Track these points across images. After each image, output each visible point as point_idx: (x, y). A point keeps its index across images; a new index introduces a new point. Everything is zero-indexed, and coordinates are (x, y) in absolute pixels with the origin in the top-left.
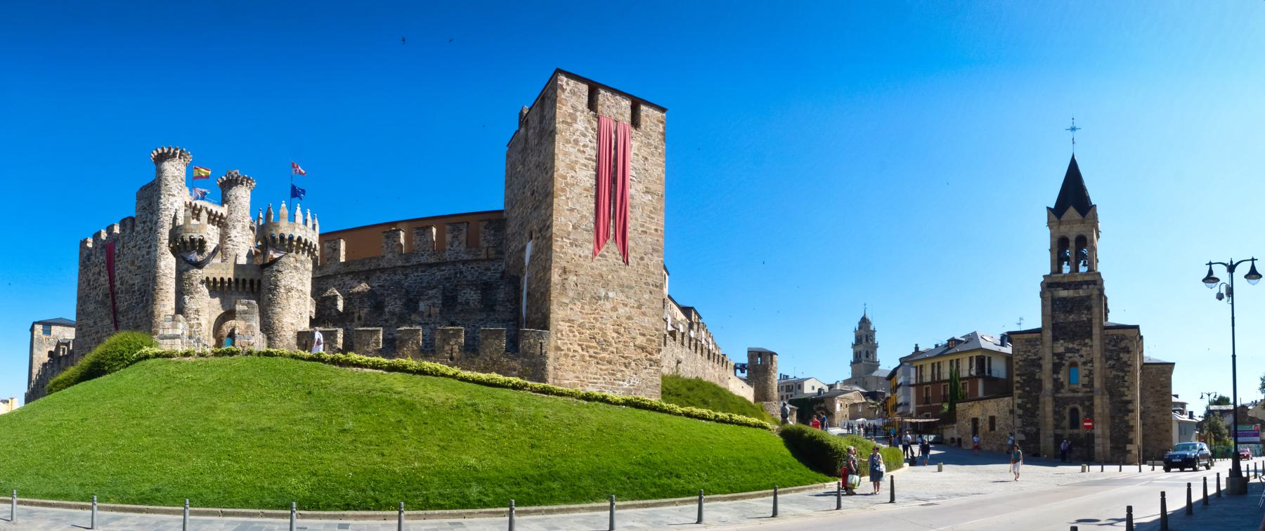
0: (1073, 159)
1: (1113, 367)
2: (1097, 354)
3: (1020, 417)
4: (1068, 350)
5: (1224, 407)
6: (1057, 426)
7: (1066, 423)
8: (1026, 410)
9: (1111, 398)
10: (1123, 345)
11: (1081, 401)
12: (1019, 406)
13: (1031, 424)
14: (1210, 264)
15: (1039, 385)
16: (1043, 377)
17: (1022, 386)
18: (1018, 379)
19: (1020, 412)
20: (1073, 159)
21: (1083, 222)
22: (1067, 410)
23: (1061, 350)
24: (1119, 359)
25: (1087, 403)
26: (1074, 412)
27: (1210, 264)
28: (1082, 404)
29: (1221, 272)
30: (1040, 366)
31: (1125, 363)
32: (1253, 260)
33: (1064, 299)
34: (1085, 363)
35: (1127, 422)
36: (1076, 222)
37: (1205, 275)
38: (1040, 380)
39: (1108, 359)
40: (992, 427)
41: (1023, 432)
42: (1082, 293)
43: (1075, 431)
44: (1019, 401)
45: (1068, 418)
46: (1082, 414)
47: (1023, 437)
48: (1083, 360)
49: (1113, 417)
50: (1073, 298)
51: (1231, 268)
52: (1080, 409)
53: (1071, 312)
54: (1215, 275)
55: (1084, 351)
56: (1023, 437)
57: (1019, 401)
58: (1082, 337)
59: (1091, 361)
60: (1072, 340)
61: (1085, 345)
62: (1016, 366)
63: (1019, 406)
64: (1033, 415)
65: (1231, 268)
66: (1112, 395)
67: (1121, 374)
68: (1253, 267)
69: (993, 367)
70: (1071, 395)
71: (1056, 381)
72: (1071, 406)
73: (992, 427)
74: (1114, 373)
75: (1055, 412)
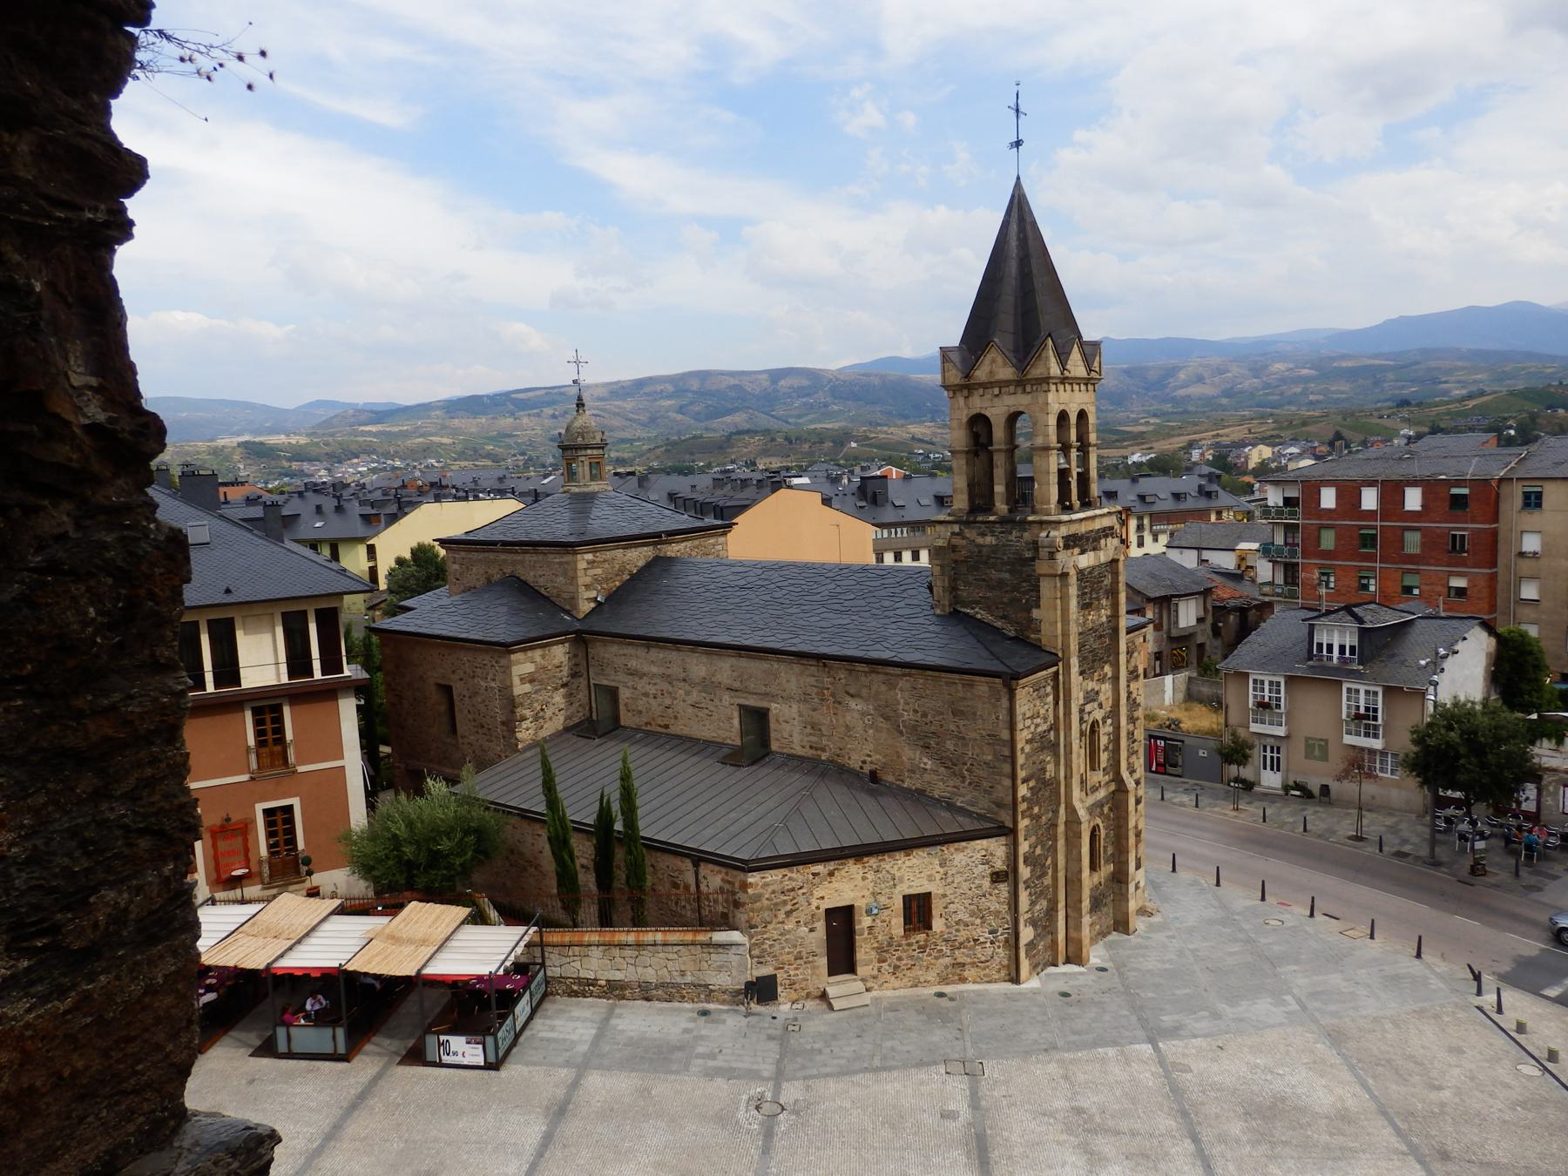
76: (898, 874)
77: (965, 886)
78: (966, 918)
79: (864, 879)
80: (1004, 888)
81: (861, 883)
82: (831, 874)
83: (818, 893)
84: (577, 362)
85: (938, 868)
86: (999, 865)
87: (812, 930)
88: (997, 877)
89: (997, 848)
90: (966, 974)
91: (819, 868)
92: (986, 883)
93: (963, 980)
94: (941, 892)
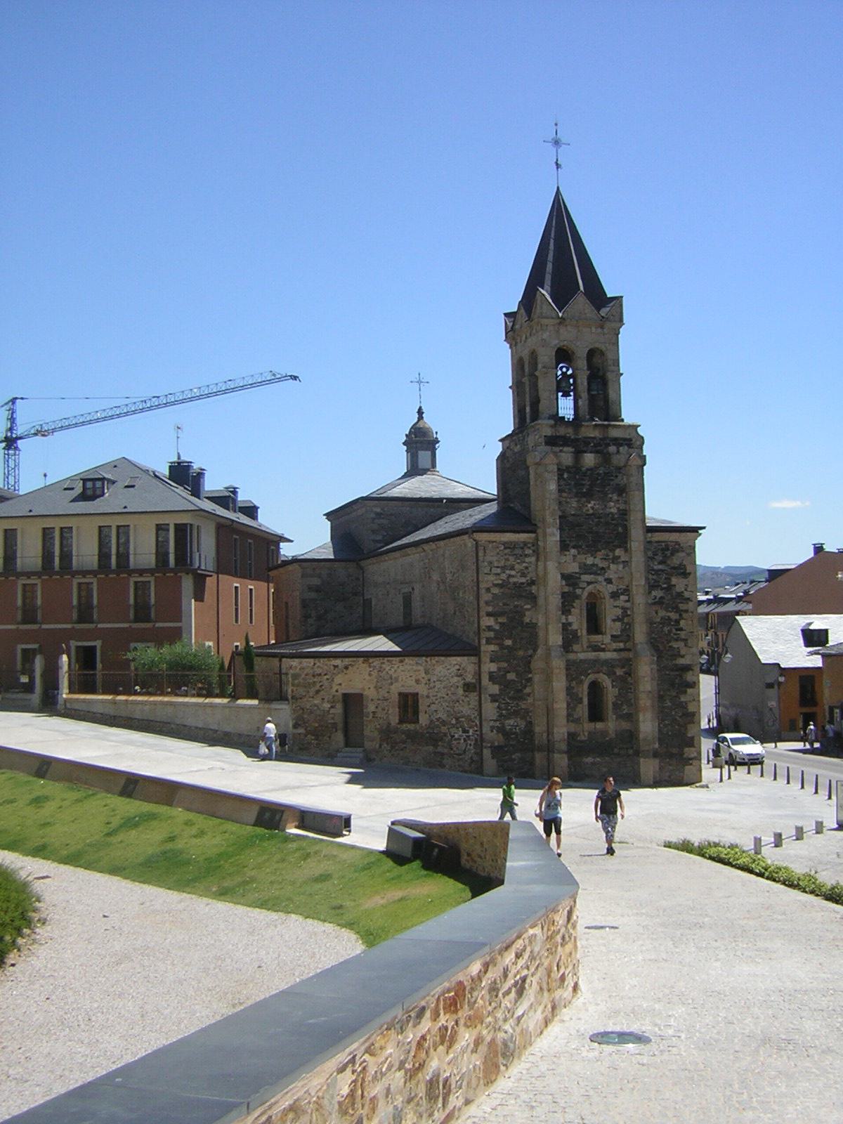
1: (659, 602)
2: (639, 582)
3: (494, 698)
4: (586, 569)
5: (603, 655)
7: (583, 710)
11: (609, 667)
12: (492, 678)
13: (516, 713)
15: (530, 636)
16: (541, 621)
17: (498, 638)
18: (490, 622)
19: (495, 689)
20: (558, 188)
23: (573, 568)
24: (670, 587)
25: (619, 672)
28: (611, 674)
30: (533, 599)
31: (680, 595)
34: (615, 595)
38: (533, 626)
43: (599, 725)
44: (493, 667)
46: (611, 692)
47: (497, 739)
48: (612, 588)
53: (589, 495)
55: (614, 571)
57: (493, 667)
59: (627, 591)
60: (592, 549)
61: (615, 560)
62: (486, 597)
63: (492, 678)
64: (519, 696)
67: (674, 616)
70: (591, 655)
71: (566, 627)
72: (592, 677)
74: (662, 613)
75: (569, 690)
76: (394, 676)
78: (444, 717)
79: (370, 675)
80: (473, 696)
81: (367, 677)
82: (346, 668)
84: (419, 382)
85: (424, 675)
86: (470, 678)
88: (468, 687)
89: (467, 663)
90: (445, 761)
91: (338, 662)
92: (461, 691)
93: (443, 766)
94: (425, 693)
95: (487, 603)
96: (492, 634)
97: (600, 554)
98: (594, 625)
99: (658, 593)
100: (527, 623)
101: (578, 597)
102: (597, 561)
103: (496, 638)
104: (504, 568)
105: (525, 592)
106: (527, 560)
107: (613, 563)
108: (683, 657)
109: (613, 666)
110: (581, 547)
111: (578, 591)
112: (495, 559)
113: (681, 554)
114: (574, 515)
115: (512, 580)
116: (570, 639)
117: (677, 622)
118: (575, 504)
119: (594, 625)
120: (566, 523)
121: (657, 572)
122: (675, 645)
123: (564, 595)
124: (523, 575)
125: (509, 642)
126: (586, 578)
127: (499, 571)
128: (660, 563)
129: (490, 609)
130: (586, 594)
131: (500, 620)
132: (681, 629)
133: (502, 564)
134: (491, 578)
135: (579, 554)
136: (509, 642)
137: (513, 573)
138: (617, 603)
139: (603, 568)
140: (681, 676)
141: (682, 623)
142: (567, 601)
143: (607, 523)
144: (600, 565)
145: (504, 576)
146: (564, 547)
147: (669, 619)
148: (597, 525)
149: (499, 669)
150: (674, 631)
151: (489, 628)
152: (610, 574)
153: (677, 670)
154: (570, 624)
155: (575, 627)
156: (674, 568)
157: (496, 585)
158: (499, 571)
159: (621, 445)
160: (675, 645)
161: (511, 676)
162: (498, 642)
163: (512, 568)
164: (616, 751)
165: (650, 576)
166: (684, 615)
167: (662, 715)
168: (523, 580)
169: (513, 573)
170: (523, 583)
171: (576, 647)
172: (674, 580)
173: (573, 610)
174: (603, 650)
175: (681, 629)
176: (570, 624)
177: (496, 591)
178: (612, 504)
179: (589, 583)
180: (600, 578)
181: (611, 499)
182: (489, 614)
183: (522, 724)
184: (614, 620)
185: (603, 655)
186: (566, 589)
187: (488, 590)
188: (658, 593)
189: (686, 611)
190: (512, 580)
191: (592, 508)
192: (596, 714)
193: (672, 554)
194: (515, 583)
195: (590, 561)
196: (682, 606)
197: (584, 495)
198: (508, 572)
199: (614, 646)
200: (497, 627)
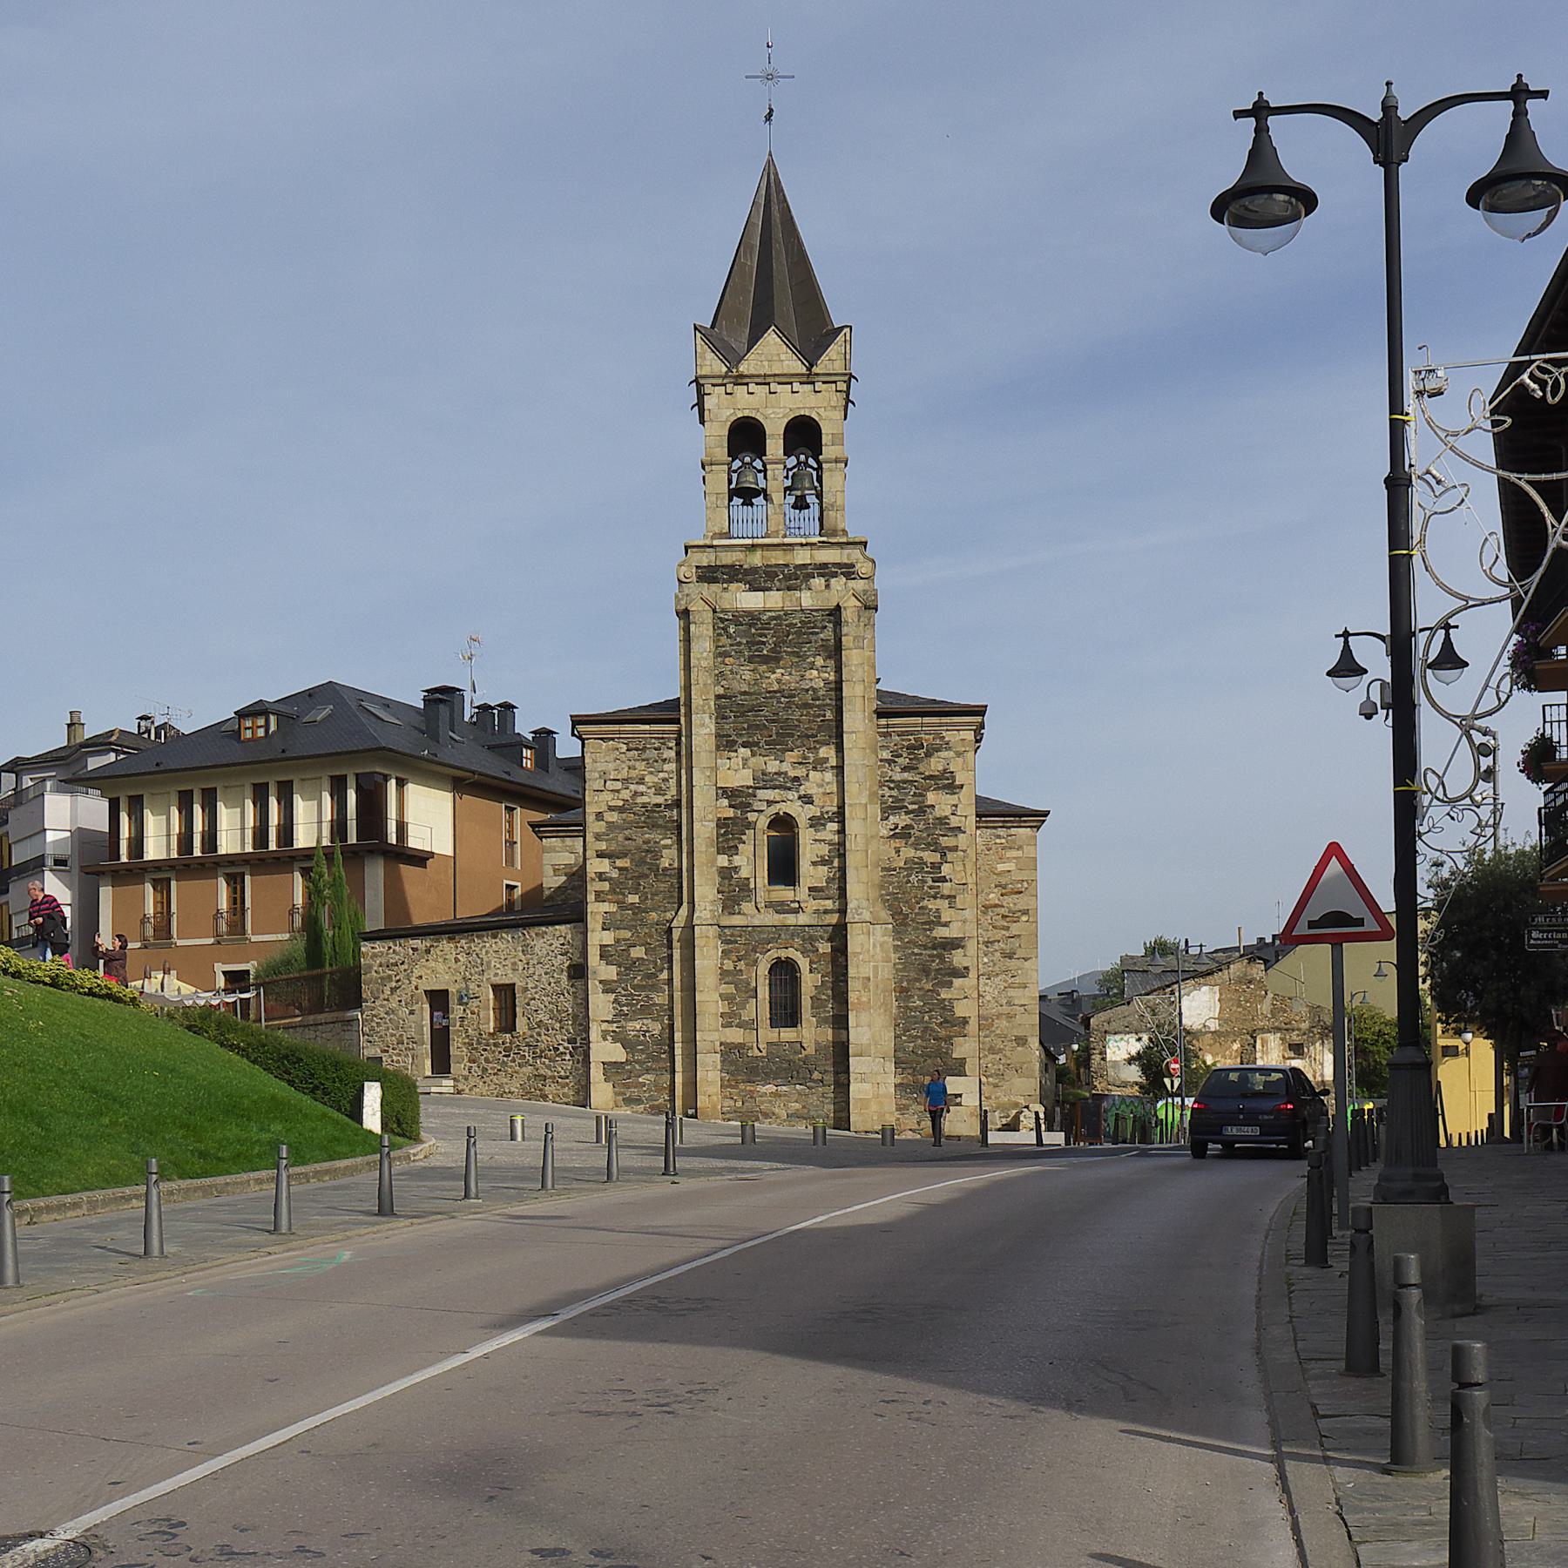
0: (770, 163)
1: (902, 834)
3: (608, 988)
4: (765, 780)
5: (791, 919)
6: (729, 1019)
7: (760, 1007)
8: (629, 967)
9: (898, 932)
10: (935, 765)
11: (806, 937)
13: (646, 1011)
14: (1260, 111)
17: (617, 889)
18: (604, 865)
19: (611, 972)
20: (770, 163)
21: (809, 379)
22: (763, 968)
23: (743, 778)
24: (922, 810)
26: (784, 973)
27: (1260, 111)
29: (1320, 155)
31: (942, 821)
32: (1519, 94)
33: (753, 617)
34: (817, 823)
35: (946, 1007)
36: (786, 379)
37: (1230, 174)
39: (887, 811)
40: (507, 1021)
41: (618, 1037)
42: (807, 599)
43: (788, 1034)
44: (608, 938)
45: (764, 992)
47: (618, 1053)
48: (813, 810)
49: (903, 993)
50: (781, 616)
51: (1388, 138)
52: (803, 963)
53: (773, 660)
54: (1296, 169)
56: (618, 1053)
57: (608, 938)
58: (809, 740)
60: (778, 745)
65: (1388, 138)
66: (901, 923)
67: (931, 857)
68: (1519, 135)
69: (409, 818)
70: (770, 918)
71: (727, 873)
73: (507, 1021)
77: (544, 978)
79: (457, 960)
83: (416, 973)
87: (412, 1012)
91: (416, 943)
93: (545, 1097)
95: (598, 837)
96: (606, 886)
97: (792, 756)
98: (783, 867)
99: (902, 820)
100: (665, 869)
101: (751, 825)
102: (786, 767)
103: (612, 891)
104: (626, 781)
105: (673, 817)
106: (666, 767)
107: (815, 769)
108: (946, 925)
109: (812, 939)
110: (757, 744)
111: (752, 817)
112: (611, 766)
113: (943, 754)
114: (745, 693)
115: (640, 800)
116: (734, 891)
117: (936, 867)
118: (747, 676)
119: (783, 867)
120: (726, 705)
121: (899, 785)
122: (931, 905)
123: (722, 823)
124: (659, 791)
125: (633, 899)
126: (761, 794)
127: (618, 785)
128: (904, 769)
129: (603, 846)
130: (763, 822)
131: (619, 863)
132: (944, 880)
133: (624, 774)
134: (607, 797)
135: (753, 754)
136: (633, 899)
137: (642, 788)
138: (819, 836)
139: (796, 779)
140: (941, 957)
141: (946, 869)
142: (730, 834)
143: (806, 706)
144: (792, 774)
145: (626, 794)
146: (725, 743)
147: (922, 862)
148: (788, 706)
149: (618, 941)
150: (930, 883)
151: (601, 877)
152: (809, 788)
153: (934, 948)
154: (736, 869)
155: (744, 873)
156: (931, 777)
157: (611, 809)
158: (618, 785)
159: (835, 575)
160: (931, 905)
161: (638, 952)
162: (614, 897)
163: (641, 781)
164: (816, 1075)
165: (887, 792)
166: (949, 856)
167: (904, 1024)
168: (660, 800)
169: (642, 788)
170: (659, 805)
171: (747, 907)
172: (931, 798)
173: (741, 846)
174: (795, 911)
175: (944, 880)
176: (736, 869)
177: (613, 817)
178: (815, 673)
179: (770, 803)
180: (793, 795)
181: (812, 666)
182: (600, 855)
183: (656, 1028)
184: (814, 864)
185: (791, 919)
186: (730, 813)
187: (599, 816)
188: (902, 820)
189: (955, 849)
190: (640, 800)
191: (779, 681)
192: (786, 1012)
193: (928, 755)
194: (644, 805)
195: (773, 766)
196: (946, 841)
197: (765, 660)
198: (632, 787)
199: (812, 905)
200: (615, 874)
